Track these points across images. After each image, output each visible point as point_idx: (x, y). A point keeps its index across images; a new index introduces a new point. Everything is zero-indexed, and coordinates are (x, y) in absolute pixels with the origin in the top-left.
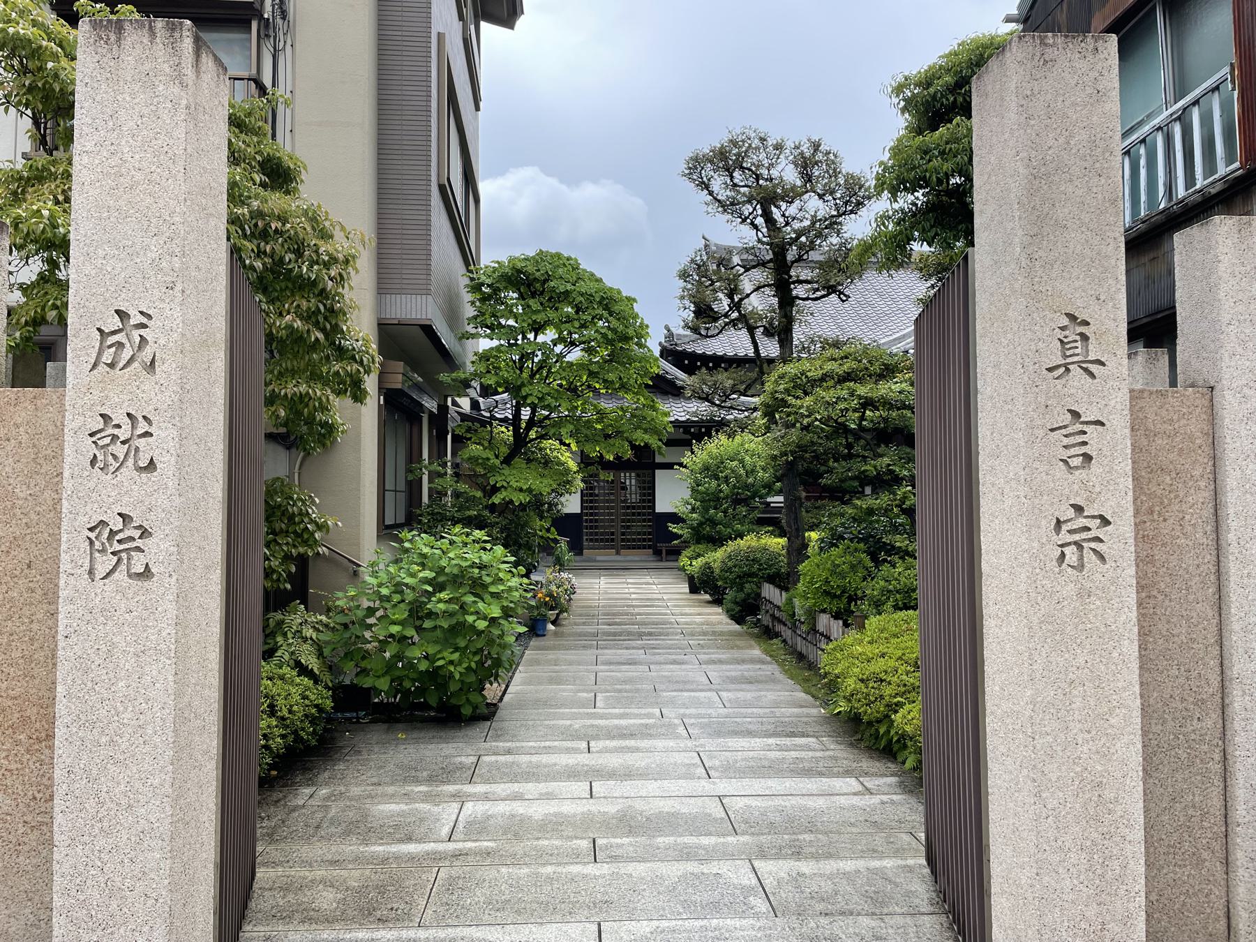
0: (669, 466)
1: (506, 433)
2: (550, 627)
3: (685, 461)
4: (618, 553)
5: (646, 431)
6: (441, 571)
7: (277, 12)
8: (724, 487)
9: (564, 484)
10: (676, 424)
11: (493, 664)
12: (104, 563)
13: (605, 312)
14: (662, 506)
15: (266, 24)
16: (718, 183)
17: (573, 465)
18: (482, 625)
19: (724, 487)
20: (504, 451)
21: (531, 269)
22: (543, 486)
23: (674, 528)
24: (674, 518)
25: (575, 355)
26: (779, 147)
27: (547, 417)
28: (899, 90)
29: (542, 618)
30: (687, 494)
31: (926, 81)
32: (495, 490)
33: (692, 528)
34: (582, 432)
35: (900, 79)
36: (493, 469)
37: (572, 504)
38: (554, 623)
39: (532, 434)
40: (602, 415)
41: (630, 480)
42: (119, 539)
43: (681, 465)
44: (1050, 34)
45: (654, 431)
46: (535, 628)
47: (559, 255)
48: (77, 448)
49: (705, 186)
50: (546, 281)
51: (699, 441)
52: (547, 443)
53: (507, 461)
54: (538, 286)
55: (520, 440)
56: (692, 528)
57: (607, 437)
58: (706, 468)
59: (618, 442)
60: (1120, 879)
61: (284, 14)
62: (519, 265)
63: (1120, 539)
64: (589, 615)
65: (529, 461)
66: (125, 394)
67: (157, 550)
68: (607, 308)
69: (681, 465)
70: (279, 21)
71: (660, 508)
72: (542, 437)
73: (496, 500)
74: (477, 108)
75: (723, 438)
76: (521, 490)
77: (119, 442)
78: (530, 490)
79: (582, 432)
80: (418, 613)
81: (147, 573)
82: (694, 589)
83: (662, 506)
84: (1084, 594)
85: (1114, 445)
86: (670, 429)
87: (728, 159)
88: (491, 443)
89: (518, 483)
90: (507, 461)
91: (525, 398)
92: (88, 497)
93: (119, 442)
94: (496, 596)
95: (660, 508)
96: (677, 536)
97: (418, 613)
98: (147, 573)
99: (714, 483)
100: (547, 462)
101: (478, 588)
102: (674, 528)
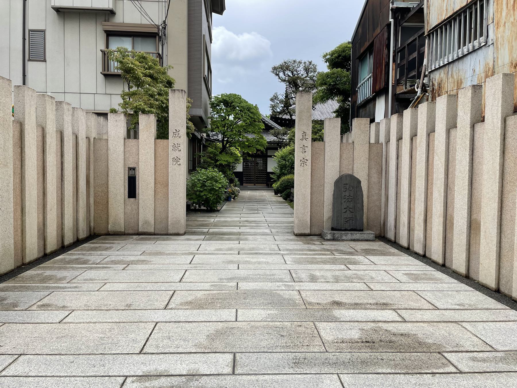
0: (271, 156)
1: (220, 145)
2: (232, 200)
3: (276, 154)
4: (255, 185)
5: (260, 145)
6: (208, 177)
7: (163, 35)
8: (287, 163)
9: (237, 160)
10: (268, 143)
11: (218, 200)
12: (175, 163)
13: (250, 111)
14: (269, 170)
15: (160, 38)
16: (281, 74)
17: (239, 155)
18: (217, 189)
19: (287, 163)
20: (220, 150)
21: (228, 99)
22: (231, 160)
23: (271, 176)
24: (272, 173)
25: (240, 123)
26: (300, 63)
27: (232, 141)
28: (325, 56)
29: (230, 197)
30: (276, 165)
31: (332, 54)
32: (217, 161)
33: (277, 176)
34: (242, 145)
35: (325, 54)
36: (217, 155)
37: (239, 168)
38: (234, 198)
39: (228, 146)
40: (248, 140)
41: (260, 161)
42: (176, 160)
43: (274, 156)
44: (283, 105)
45: (262, 145)
46: (228, 199)
47: (235, 95)
48: (170, 148)
49: (277, 75)
50: (232, 103)
51: (280, 148)
52: (232, 148)
53: (221, 153)
54: (229, 102)
55: (224, 147)
56: (277, 176)
57: (249, 147)
58: (282, 157)
59: (252, 148)
60: (307, 207)
61: (165, 35)
62: (225, 98)
63: (309, 163)
64: (243, 198)
65: (226, 153)
66: (177, 141)
67: (181, 161)
68: (248, 111)
69: (274, 156)
70: (163, 37)
71: (268, 171)
72: (230, 146)
73: (218, 163)
74: (211, 43)
75: (288, 147)
76: (225, 161)
77: (176, 147)
78: (227, 161)
79: (242, 145)
80: (203, 185)
81: (180, 164)
82: (276, 193)
83: (269, 170)
84: (304, 170)
85: (309, 150)
86: (267, 144)
87: (284, 67)
88: (216, 148)
89: (224, 159)
90: (221, 153)
91: (226, 136)
92: (173, 154)
93: (176, 147)
94: (220, 183)
95: (268, 171)
96: (273, 179)
97: (203, 185)
98: (180, 164)
99: (284, 161)
100: (232, 154)
101: (216, 181)
102: (271, 176)
